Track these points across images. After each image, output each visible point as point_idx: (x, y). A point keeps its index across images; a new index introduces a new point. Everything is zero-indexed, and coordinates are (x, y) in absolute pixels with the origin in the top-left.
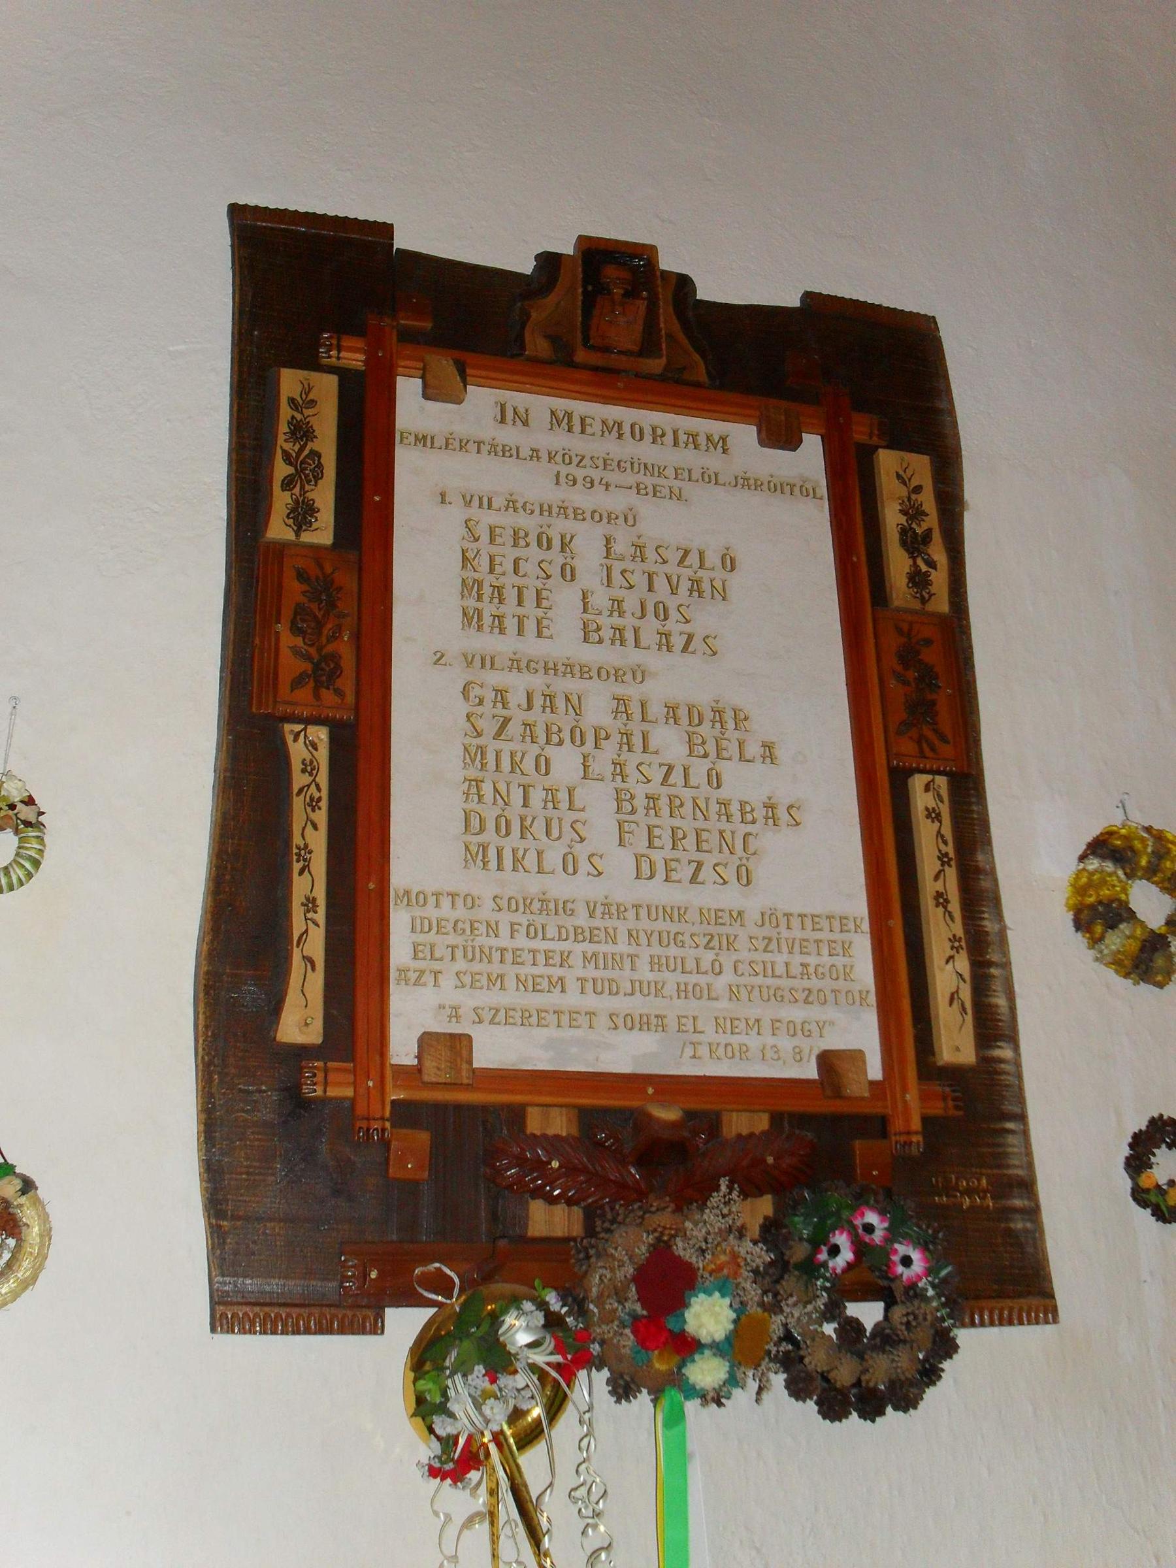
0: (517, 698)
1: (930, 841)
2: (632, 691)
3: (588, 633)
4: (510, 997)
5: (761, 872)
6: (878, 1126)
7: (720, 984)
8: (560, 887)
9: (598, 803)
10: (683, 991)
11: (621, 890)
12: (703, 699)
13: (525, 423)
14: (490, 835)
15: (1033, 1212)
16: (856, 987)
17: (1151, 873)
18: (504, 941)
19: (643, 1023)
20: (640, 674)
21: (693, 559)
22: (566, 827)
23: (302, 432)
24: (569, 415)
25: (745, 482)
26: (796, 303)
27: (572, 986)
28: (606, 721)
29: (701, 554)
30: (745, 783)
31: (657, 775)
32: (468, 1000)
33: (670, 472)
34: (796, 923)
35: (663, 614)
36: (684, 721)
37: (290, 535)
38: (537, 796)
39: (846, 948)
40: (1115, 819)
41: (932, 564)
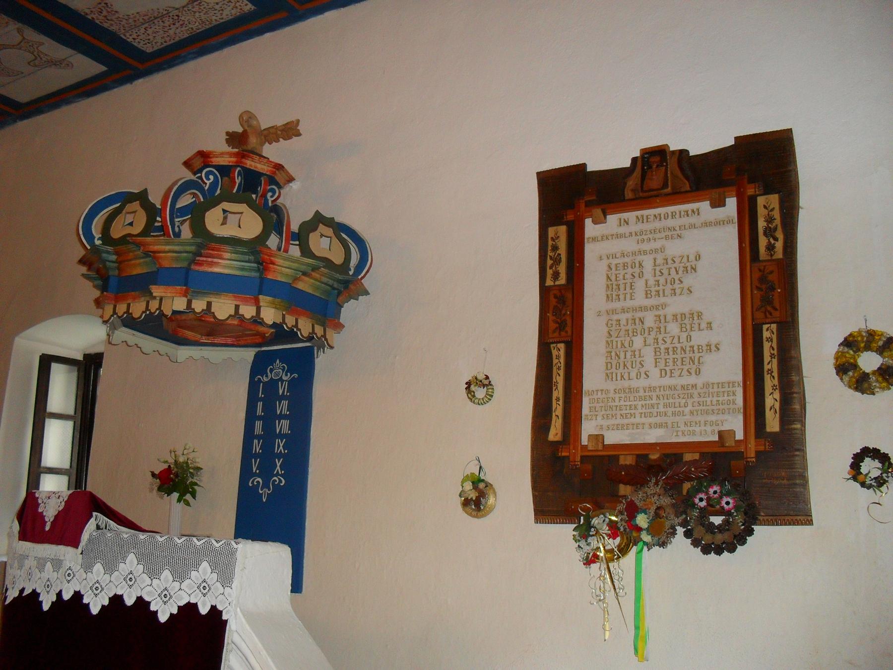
1: (768, 349)
2: (661, 312)
3: (647, 295)
4: (619, 421)
6: (739, 455)
7: (687, 410)
8: (634, 384)
10: (674, 414)
11: (666, 382)
12: (686, 310)
13: (627, 224)
14: (614, 370)
16: (736, 407)
17: (868, 348)
18: (617, 403)
19: (660, 426)
20: (664, 306)
21: (685, 260)
22: (638, 363)
23: (555, 248)
24: (642, 216)
25: (706, 224)
27: (638, 416)
28: (652, 324)
29: (688, 257)
30: (699, 338)
31: (668, 340)
32: (605, 423)
33: (677, 228)
34: (715, 386)
35: (673, 282)
36: (679, 319)
37: (552, 284)
38: (629, 354)
39: (734, 394)
41: (776, 239)
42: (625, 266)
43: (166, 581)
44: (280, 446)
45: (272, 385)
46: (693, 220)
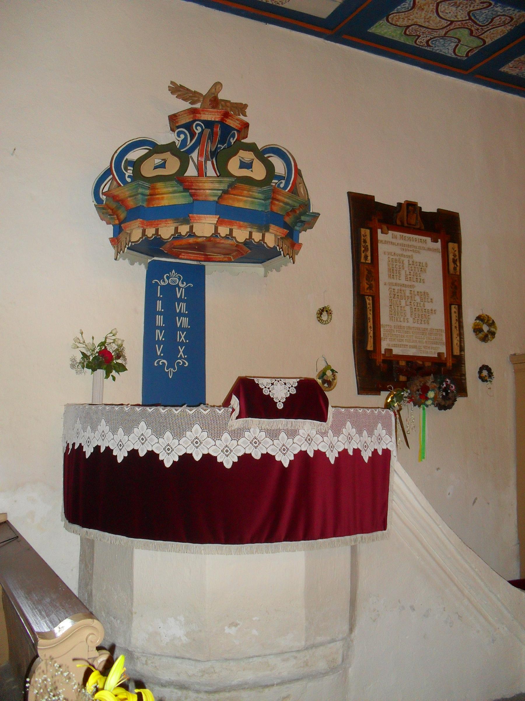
0: (396, 291)
1: (454, 316)
3: (406, 279)
5: (430, 322)
9: (408, 309)
15: (465, 379)
17: (486, 323)
20: (413, 286)
23: (365, 241)
25: (429, 249)
26: (436, 211)
27: (404, 341)
28: (409, 295)
31: (416, 304)
37: (364, 261)
40: (481, 313)
41: (457, 266)
42: (396, 261)
43: (168, 439)
44: (181, 337)
45: (170, 289)
46: (424, 245)
